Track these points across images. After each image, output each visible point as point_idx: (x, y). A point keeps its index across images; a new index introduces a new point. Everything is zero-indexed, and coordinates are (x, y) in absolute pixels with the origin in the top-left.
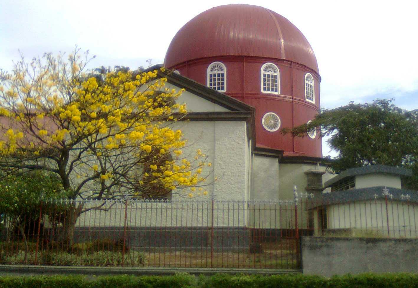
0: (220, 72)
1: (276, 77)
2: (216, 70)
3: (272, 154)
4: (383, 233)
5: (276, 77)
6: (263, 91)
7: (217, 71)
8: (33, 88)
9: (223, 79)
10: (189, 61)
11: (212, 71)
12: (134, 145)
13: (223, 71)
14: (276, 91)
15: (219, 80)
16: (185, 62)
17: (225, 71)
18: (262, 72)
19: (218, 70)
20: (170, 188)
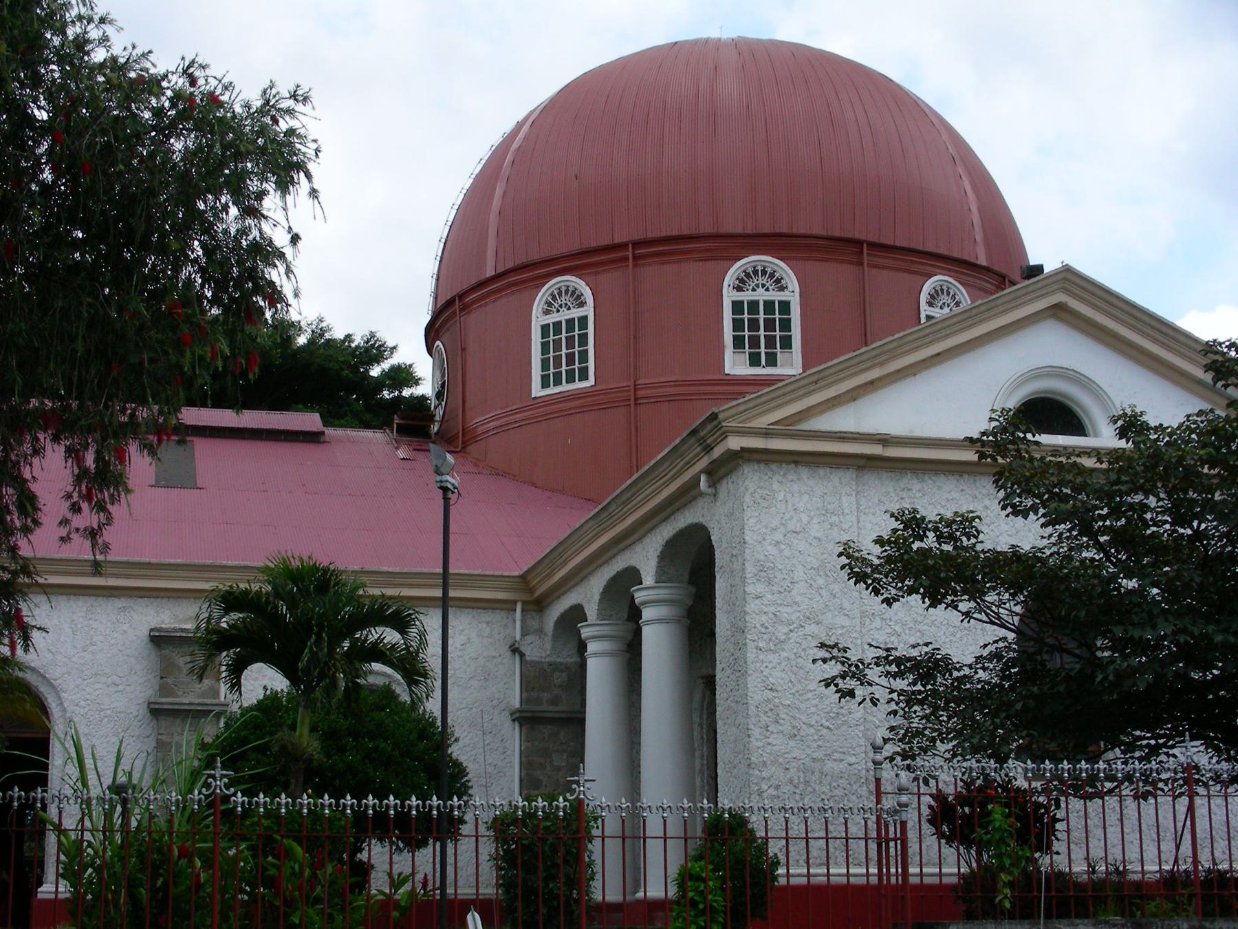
0: (776, 296)
1: (785, 307)
2: (757, 286)
3: (1095, 387)
4: (840, 479)
5: (785, 307)
6: (591, 381)
7: (761, 290)
8: (1231, 631)
9: (786, 325)
10: (637, 244)
11: (547, 312)
12: (381, 697)
13: (786, 292)
14: (545, 383)
15: (770, 325)
16: (622, 246)
17: (792, 294)
18: (729, 296)
19: (569, 309)
20: (378, 715)
